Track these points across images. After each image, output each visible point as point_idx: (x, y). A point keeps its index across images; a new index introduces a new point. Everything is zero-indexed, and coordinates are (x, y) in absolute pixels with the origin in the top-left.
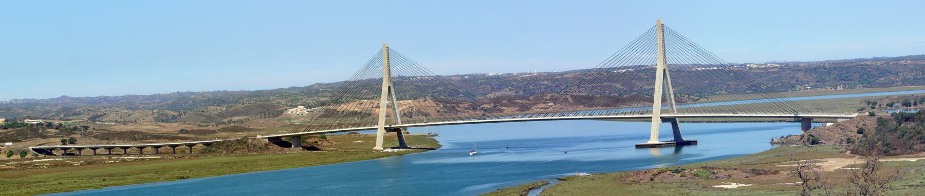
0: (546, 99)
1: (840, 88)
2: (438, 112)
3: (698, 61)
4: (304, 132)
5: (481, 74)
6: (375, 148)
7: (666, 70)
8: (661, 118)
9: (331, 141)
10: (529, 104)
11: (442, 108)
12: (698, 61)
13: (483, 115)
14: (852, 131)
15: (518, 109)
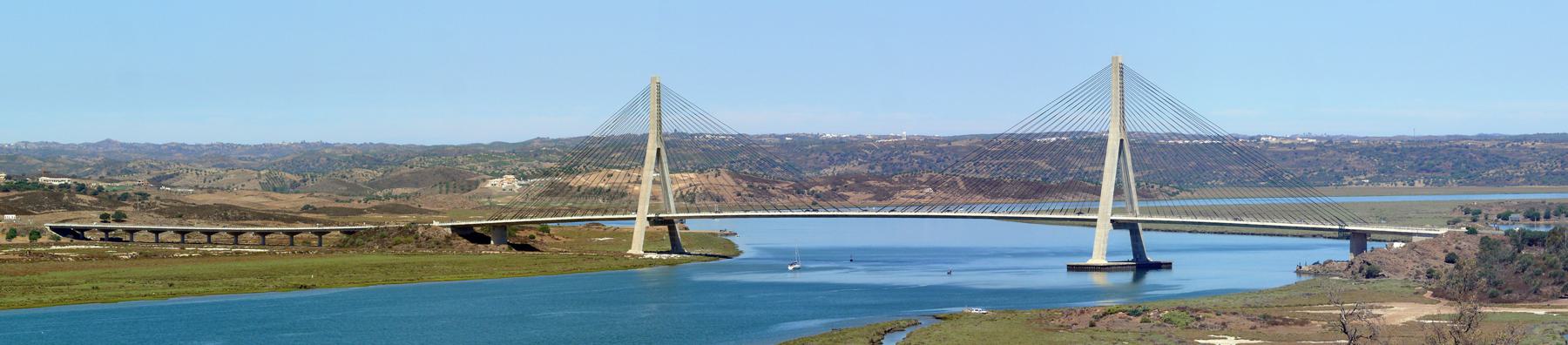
2: (739, 195)
6: (629, 252)
10: (891, 189)
13: (814, 204)
15: (871, 195)
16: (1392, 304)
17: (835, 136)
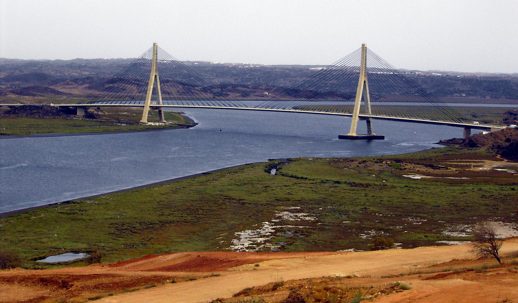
0: (261, 89)
1: (488, 98)
2: (178, 92)
3: (378, 66)
4: (87, 104)
5: (207, 62)
6: (141, 121)
7: (366, 82)
8: (359, 117)
9: (104, 112)
10: (248, 92)
11: (181, 90)
12: (378, 66)
13: (214, 98)
14: (501, 140)
15: (240, 94)
16: (485, 161)
17: (217, 63)
